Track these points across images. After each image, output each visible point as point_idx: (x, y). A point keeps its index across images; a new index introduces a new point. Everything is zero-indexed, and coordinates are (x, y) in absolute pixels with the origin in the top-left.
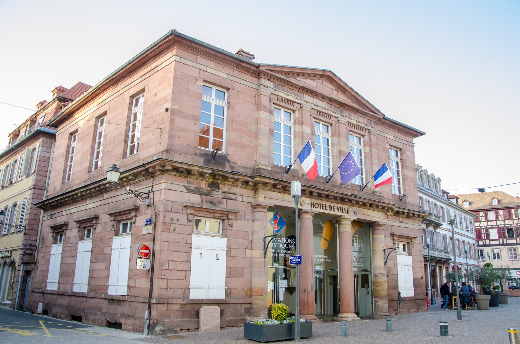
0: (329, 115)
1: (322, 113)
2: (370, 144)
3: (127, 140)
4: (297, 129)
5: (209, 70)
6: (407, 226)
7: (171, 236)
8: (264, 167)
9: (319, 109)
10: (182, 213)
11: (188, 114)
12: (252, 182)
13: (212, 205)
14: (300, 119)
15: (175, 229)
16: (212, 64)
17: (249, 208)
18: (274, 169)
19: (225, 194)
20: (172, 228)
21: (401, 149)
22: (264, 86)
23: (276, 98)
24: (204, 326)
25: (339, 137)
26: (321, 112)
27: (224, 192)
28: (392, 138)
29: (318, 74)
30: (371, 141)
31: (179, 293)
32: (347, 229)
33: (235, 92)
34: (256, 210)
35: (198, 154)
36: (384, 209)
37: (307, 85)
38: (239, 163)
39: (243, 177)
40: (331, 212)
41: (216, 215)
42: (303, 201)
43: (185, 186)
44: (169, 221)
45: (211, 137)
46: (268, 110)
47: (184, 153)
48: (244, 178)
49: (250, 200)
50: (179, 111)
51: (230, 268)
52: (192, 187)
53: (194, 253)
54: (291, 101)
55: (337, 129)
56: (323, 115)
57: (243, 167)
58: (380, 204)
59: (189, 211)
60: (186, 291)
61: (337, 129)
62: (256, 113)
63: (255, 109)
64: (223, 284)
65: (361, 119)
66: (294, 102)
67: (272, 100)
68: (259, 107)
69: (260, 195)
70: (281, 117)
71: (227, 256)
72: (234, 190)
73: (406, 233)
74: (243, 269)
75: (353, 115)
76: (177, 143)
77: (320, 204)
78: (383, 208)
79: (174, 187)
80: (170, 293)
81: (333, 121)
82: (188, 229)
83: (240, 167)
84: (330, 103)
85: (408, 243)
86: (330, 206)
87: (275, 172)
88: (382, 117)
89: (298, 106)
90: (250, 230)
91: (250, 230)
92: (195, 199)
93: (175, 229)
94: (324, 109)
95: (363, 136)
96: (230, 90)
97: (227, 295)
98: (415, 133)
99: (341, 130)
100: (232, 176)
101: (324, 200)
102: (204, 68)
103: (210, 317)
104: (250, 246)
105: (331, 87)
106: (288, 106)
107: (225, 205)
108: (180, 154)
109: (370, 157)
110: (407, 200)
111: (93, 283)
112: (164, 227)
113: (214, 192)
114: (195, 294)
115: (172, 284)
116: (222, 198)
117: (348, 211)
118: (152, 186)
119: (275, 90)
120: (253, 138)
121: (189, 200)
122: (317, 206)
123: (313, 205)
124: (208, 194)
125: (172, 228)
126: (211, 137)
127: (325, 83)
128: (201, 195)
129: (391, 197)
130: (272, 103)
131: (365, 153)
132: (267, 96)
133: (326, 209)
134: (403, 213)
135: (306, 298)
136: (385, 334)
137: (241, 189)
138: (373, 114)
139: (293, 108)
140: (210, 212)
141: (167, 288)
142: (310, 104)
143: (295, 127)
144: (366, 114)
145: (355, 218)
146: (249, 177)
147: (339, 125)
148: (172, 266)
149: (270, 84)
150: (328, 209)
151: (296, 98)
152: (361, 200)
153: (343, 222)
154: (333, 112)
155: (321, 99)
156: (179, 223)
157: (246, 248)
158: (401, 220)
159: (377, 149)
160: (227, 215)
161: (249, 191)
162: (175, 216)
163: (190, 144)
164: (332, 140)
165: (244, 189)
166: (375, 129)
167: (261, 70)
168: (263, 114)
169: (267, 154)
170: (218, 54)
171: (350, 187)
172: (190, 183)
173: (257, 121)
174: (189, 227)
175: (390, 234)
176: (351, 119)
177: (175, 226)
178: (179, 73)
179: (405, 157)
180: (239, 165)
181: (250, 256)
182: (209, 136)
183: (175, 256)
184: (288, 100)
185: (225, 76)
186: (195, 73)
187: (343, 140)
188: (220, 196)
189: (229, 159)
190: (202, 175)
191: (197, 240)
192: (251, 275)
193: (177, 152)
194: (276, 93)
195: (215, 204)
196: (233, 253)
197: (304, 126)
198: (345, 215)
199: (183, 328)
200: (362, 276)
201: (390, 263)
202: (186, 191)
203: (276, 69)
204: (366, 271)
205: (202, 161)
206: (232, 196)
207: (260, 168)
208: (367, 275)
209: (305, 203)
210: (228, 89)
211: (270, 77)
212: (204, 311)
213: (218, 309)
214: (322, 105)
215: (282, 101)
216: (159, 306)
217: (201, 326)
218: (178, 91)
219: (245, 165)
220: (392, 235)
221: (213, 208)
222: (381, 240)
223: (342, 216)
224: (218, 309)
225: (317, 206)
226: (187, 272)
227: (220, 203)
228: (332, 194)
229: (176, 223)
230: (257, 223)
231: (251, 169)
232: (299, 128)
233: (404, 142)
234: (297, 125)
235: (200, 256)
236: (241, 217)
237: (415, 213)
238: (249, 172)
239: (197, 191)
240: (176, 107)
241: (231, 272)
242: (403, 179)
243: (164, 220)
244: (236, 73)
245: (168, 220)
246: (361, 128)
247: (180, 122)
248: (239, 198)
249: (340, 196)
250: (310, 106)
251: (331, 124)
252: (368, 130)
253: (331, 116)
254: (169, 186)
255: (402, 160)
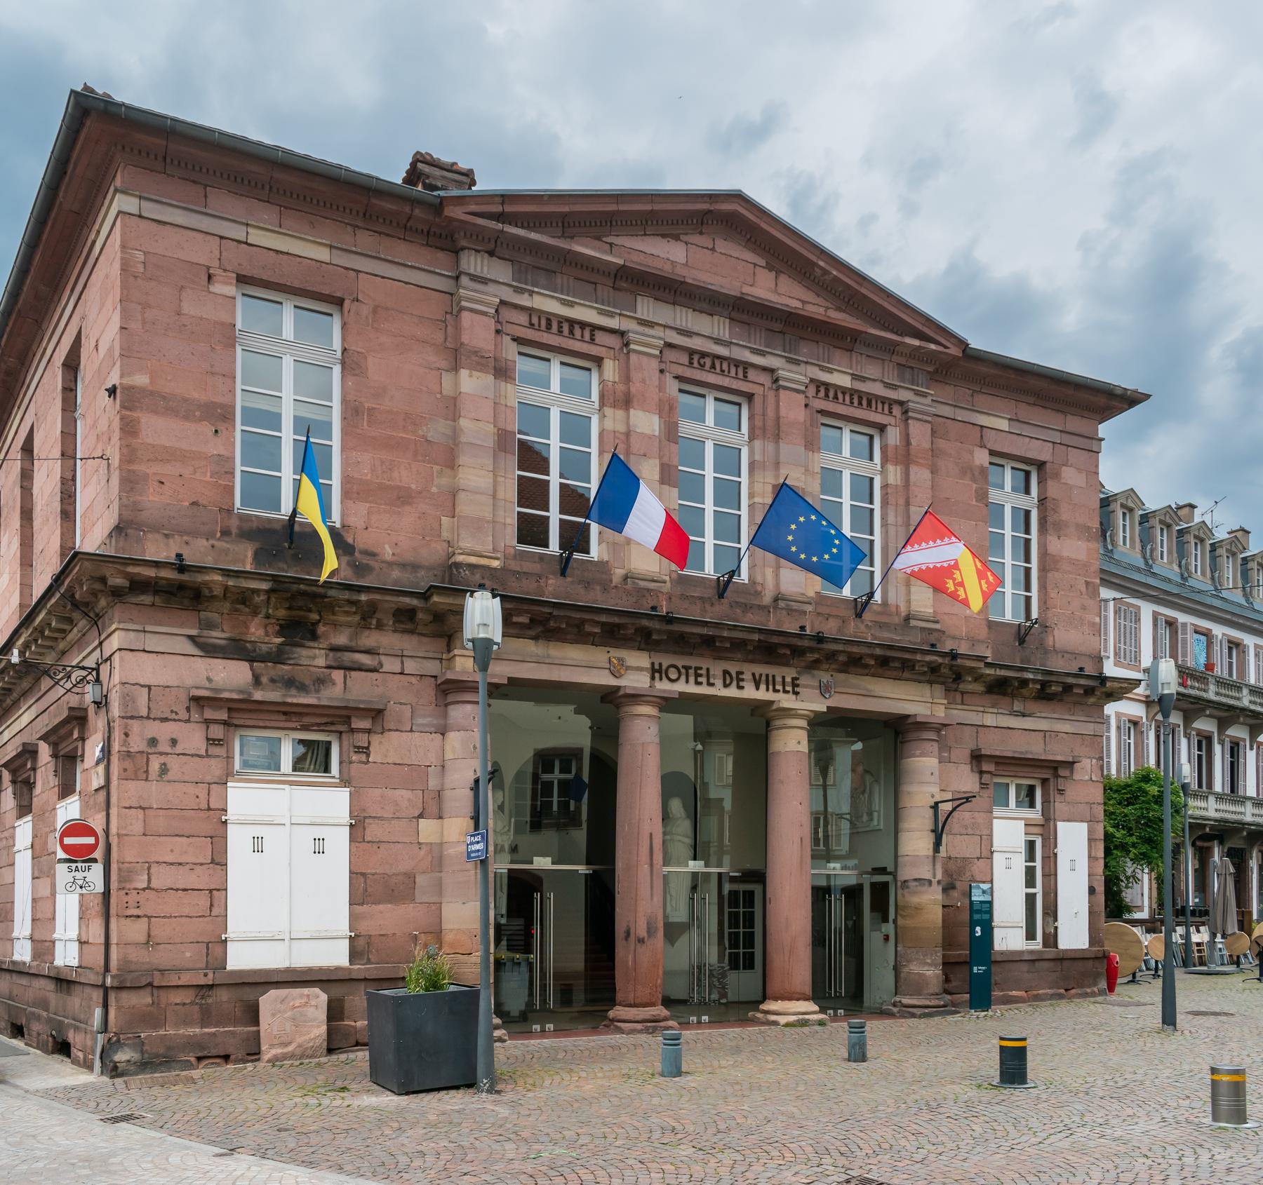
0: (737, 363)
1: (708, 362)
2: (904, 456)
3: (70, 508)
4: (891, 480)
5: (256, 237)
6: (1043, 725)
7: (154, 792)
8: (473, 560)
9: (696, 343)
10: (188, 721)
11: (185, 400)
12: (427, 610)
13: (293, 692)
14: (621, 388)
15: (164, 770)
16: (268, 214)
17: (429, 692)
18: (514, 565)
19: (339, 654)
20: (155, 765)
21: (1041, 465)
22: (474, 278)
23: (523, 319)
24: (272, 1046)
25: (777, 437)
26: (703, 355)
27: (334, 649)
28: (1003, 425)
29: (693, 214)
30: (908, 443)
31: (189, 955)
32: (792, 743)
33: (365, 310)
34: (450, 698)
35: (234, 531)
36: (948, 672)
37: (650, 261)
38: (388, 552)
39: (388, 598)
40: (732, 692)
41: (307, 720)
42: (620, 660)
43: (190, 637)
44: (142, 746)
45: (554, 515)
46: (492, 363)
47: (182, 533)
48: (395, 599)
49: (432, 667)
50: (152, 393)
51: (363, 874)
52: (217, 636)
53: (238, 840)
54: (583, 325)
55: (771, 413)
56: (713, 367)
57: (403, 566)
58: (919, 657)
59: (210, 714)
60: (217, 950)
61: (771, 413)
62: (447, 379)
63: (443, 364)
64: (342, 926)
65: (871, 370)
66: (595, 328)
67: (509, 328)
68: (457, 356)
69: (456, 652)
70: (708, 423)
71: (352, 839)
72: (370, 639)
73: (1036, 749)
74: (411, 877)
75: (838, 354)
76: (153, 499)
77: (687, 668)
78: (934, 669)
79: (152, 643)
80: (162, 957)
81: (757, 383)
82: (214, 768)
83: (390, 564)
84: (744, 317)
85: (1044, 782)
86: (726, 672)
87: (515, 573)
88: (954, 351)
89: (613, 341)
90: (432, 758)
91: (432, 758)
92: (231, 675)
93: (164, 770)
94: (718, 341)
95: (882, 428)
96: (347, 304)
97: (354, 955)
98: (1101, 400)
99: (783, 412)
100: (346, 595)
101: (702, 656)
102: (238, 232)
103: (294, 1020)
104: (434, 807)
105: (749, 256)
106: (572, 344)
107: (338, 690)
108: (167, 536)
109: (901, 501)
110: (1050, 641)
111: (375, 864)
112: (127, 764)
113: (299, 650)
114: (240, 958)
115: (162, 930)
116: (328, 667)
117: (794, 685)
118: (101, 643)
119: (519, 291)
120: (436, 468)
121: (209, 680)
122: (673, 676)
123: (656, 672)
124: (277, 657)
125: (155, 765)
126: (554, 515)
127: (722, 246)
128: (251, 660)
129: (983, 633)
130: (507, 339)
131: (885, 487)
132: (484, 314)
133: (710, 684)
134: (1024, 683)
135: (630, 958)
136: (1132, 987)
137: (398, 635)
138: (916, 343)
139: (745, 387)
140: (285, 713)
141: (148, 942)
142: (658, 332)
143: (603, 417)
144: (890, 349)
145: (821, 707)
146: (411, 594)
147: (777, 396)
148: (162, 878)
149: (500, 271)
150: (719, 682)
151: (601, 312)
152: (840, 647)
153: (778, 723)
154: (755, 351)
155: (705, 306)
156: (179, 749)
157: (421, 816)
158: (1018, 706)
159: (934, 471)
160: (349, 718)
161: (425, 640)
162: (163, 731)
163: (202, 501)
164: (751, 453)
165: (406, 637)
166: (928, 400)
167: (451, 220)
168: (471, 382)
169: (489, 516)
170: (279, 175)
171: (809, 608)
172: (210, 626)
173: (452, 407)
174: (213, 762)
175: (967, 753)
176: (830, 371)
177: (163, 759)
178: (140, 256)
179: (1053, 490)
180: (388, 557)
181: (434, 839)
182: (548, 511)
183: (168, 849)
184: (572, 322)
185: (323, 254)
186: (202, 252)
187: (791, 449)
188: (321, 662)
189: (350, 540)
190: (243, 599)
191: (243, 799)
192: (440, 893)
193: (155, 529)
194: (524, 300)
195: (302, 688)
196: (374, 831)
197: (632, 411)
198: (786, 701)
199: (205, 1053)
200: (873, 885)
201: (955, 845)
202: (196, 651)
203: (509, 209)
204: (882, 871)
205: (250, 554)
206: (365, 659)
207: (458, 565)
208: (885, 885)
209: (628, 668)
210: (339, 302)
211: (494, 247)
212: (269, 1001)
213: (320, 997)
214: (709, 330)
215: (549, 326)
216: (124, 995)
217: (264, 1048)
218: (144, 322)
219: (409, 557)
220: (977, 758)
221: (289, 700)
222: (929, 777)
223: (772, 702)
224: (320, 997)
225: (673, 676)
226: (216, 893)
227: (321, 682)
228: (725, 634)
229: (169, 750)
230: (453, 737)
231: (430, 568)
232: (615, 420)
233: (1057, 437)
234: (608, 411)
235: (258, 845)
236: (399, 721)
237: (1070, 680)
238: (423, 581)
239: (237, 650)
240: (141, 380)
241: (365, 889)
242: (1043, 569)
243: (125, 743)
244: (365, 240)
245: (137, 744)
246: (870, 401)
247: (158, 430)
248: (390, 665)
249: (756, 637)
250: (658, 336)
251: (750, 397)
252: (901, 403)
253: (747, 366)
254: (132, 639)
255: (1042, 501)
